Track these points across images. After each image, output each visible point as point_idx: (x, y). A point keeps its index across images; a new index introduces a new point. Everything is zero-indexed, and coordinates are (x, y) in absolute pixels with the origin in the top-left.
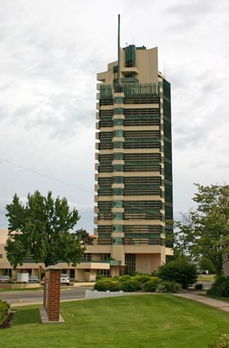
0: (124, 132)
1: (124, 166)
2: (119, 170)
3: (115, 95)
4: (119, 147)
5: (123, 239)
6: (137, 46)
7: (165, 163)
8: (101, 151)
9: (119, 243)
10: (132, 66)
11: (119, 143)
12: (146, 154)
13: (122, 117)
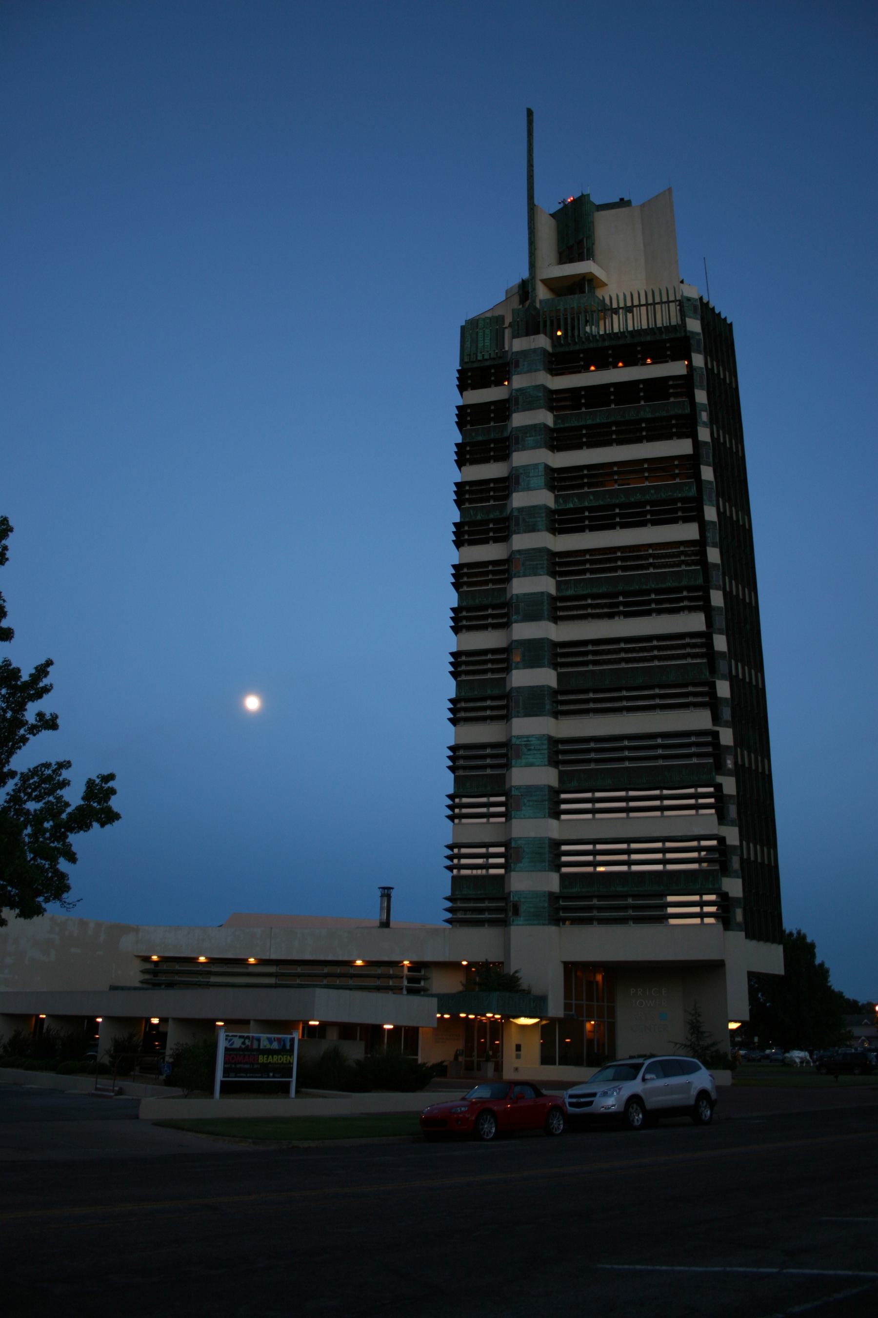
0: (554, 742)
1: (554, 599)
2: (532, 617)
3: (519, 345)
4: (533, 529)
5: (553, 897)
6: (597, 200)
7: (739, 773)
8: (466, 549)
9: (536, 918)
10: (581, 259)
11: (532, 510)
12: (650, 638)
13: (546, 418)
